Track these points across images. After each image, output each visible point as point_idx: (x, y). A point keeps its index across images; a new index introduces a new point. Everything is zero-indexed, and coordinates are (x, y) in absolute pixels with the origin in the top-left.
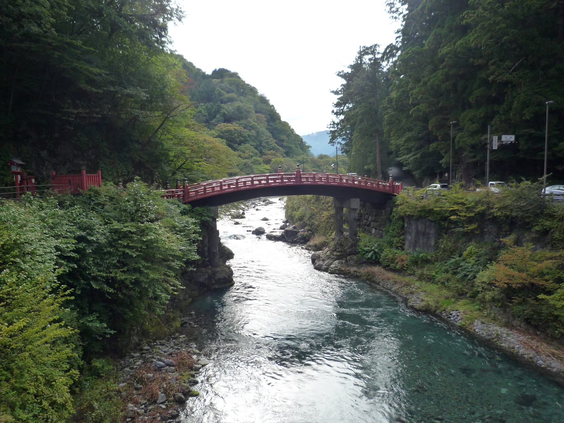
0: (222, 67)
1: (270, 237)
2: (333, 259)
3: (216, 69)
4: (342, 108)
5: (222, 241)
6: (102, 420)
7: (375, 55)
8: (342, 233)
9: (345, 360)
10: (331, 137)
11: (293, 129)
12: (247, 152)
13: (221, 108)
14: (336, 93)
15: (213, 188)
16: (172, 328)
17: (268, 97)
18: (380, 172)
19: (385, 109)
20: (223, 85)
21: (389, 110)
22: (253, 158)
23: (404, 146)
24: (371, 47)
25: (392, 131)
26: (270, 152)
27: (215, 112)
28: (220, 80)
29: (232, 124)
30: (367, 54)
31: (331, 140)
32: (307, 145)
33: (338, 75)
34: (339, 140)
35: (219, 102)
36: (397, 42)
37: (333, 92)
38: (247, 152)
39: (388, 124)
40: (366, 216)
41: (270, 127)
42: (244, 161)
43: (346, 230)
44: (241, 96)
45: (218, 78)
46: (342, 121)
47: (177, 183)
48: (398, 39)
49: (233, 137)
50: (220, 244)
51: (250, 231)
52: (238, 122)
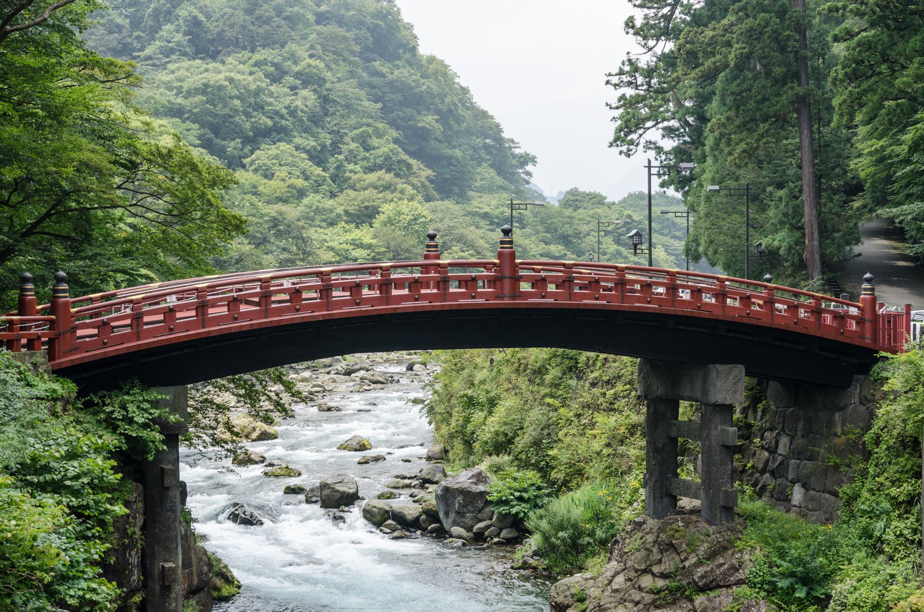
4: (666, 10)
6: (749, 607)
8: (674, 500)
11: (465, 91)
12: (282, 172)
18: (818, 263)
21: (850, 23)
22: (305, 201)
23: (907, 162)
25: (861, 106)
26: (372, 177)
31: (620, 130)
32: (517, 151)
34: (654, 134)
38: (282, 172)
39: (853, 77)
42: (272, 210)
43: (688, 490)
46: (668, 60)
50: (190, 538)
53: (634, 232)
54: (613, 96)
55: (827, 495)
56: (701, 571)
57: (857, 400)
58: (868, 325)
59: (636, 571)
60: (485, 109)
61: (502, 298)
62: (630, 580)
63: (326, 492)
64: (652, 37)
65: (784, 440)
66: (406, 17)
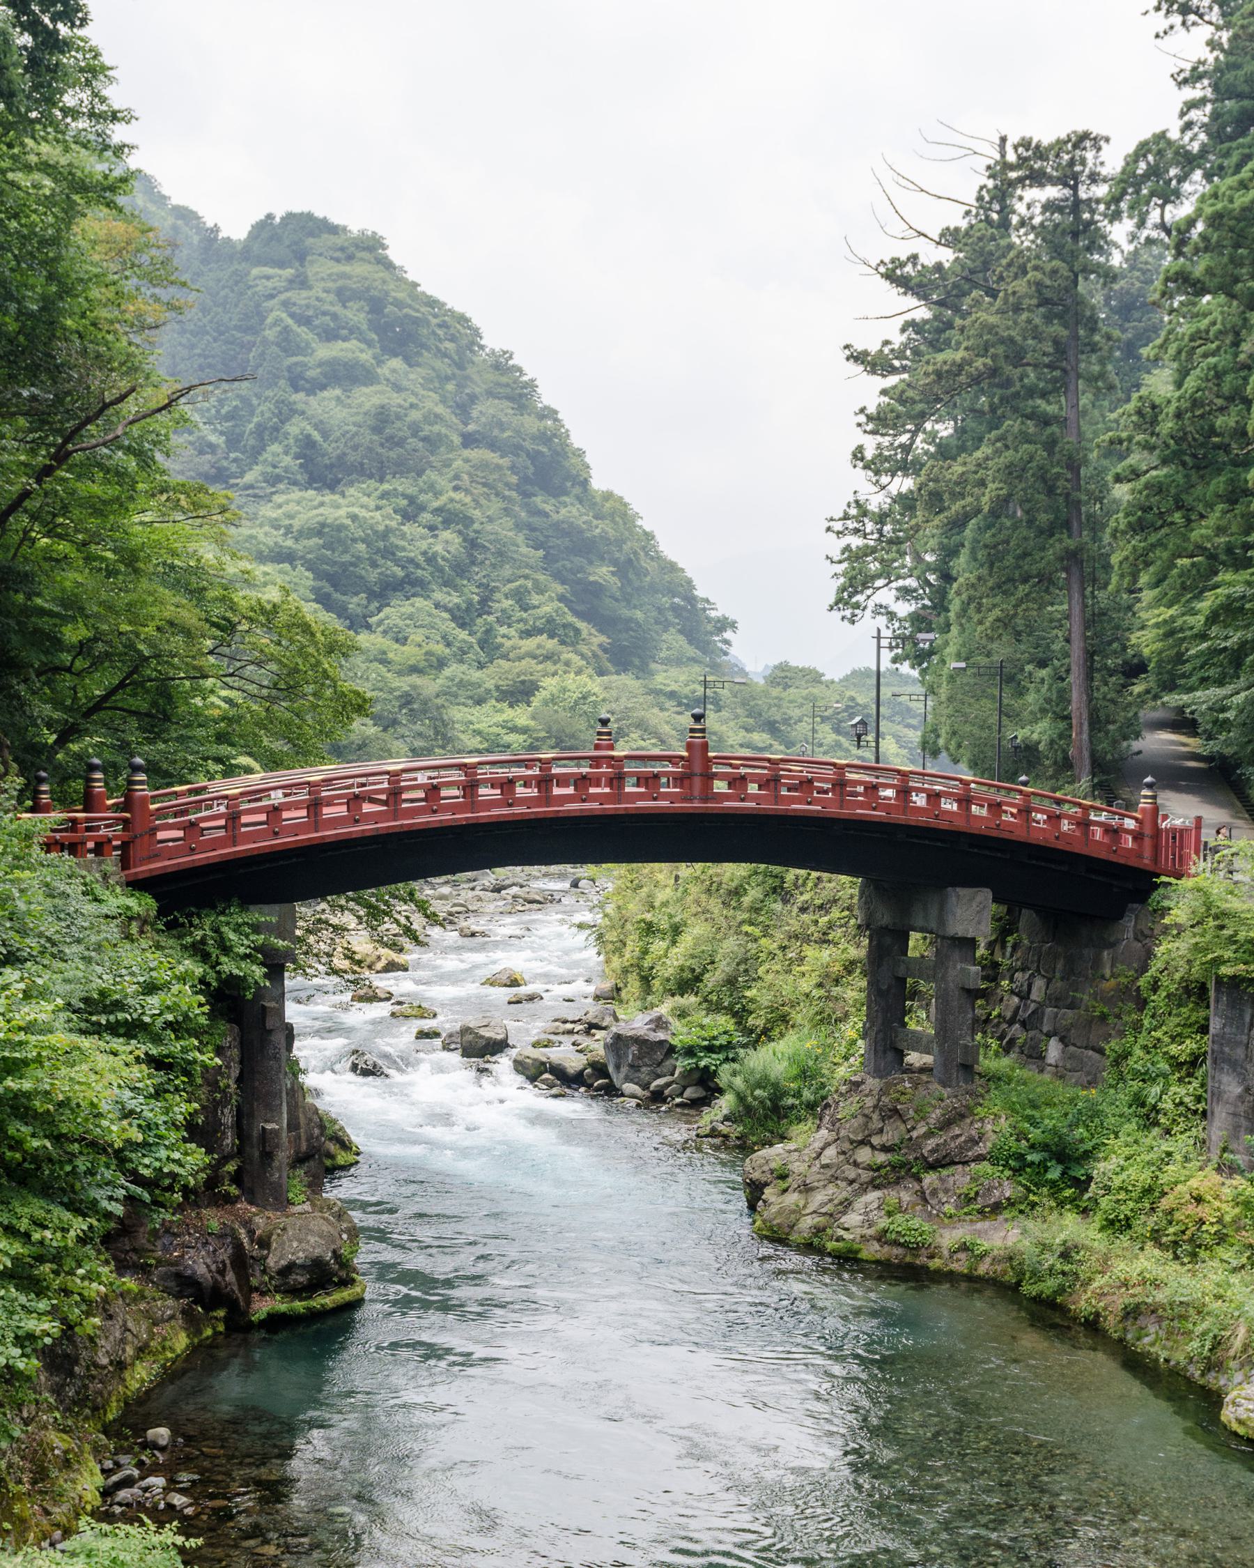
1: (533, 1072)
2: (851, 1182)
3: (270, 217)
4: (904, 439)
5: (310, 1080)
7: (1075, 188)
8: (900, 1055)
12: (417, 636)
13: (293, 412)
15: (275, 811)
16: (56, 1503)
17: (530, 364)
18: (1087, 762)
19: (1116, 448)
20: (299, 297)
21: (1137, 458)
22: (447, 672)
24: (1060, 144)
26: (530, 644)
27: (260, 430)
28: (289, 272)
29: (343, 495)
30: (1038, 178)
32: (713, 614)
33: (890, 276)
35: (282, 382)
36: (1188, 126)
37: (858, 357)
39: (1139, 527)
40: (1018, 975)
41: (536, 521)
42: (403, 684)
43: (918, 1043)
44: (395, 354)
45: (281, 265)
46: (906, 502)
47: (89, 780)
48: (1195, 115)
49: (346, 558)
50: (297, 1091)
51: (434, 1034)
52: (372, 483)
53: (857, 719)
54: (835, 546)
55: (1091, 1053)
56: (931, 1143)
57: (1131, 935)
58: (1147, 842)
59: (852, 1142)
61: (691, 801)
62: (844, 1153)
63: (469, 1037)
64: (886, 472)
65: (1039, 983)
66: (576, 441)
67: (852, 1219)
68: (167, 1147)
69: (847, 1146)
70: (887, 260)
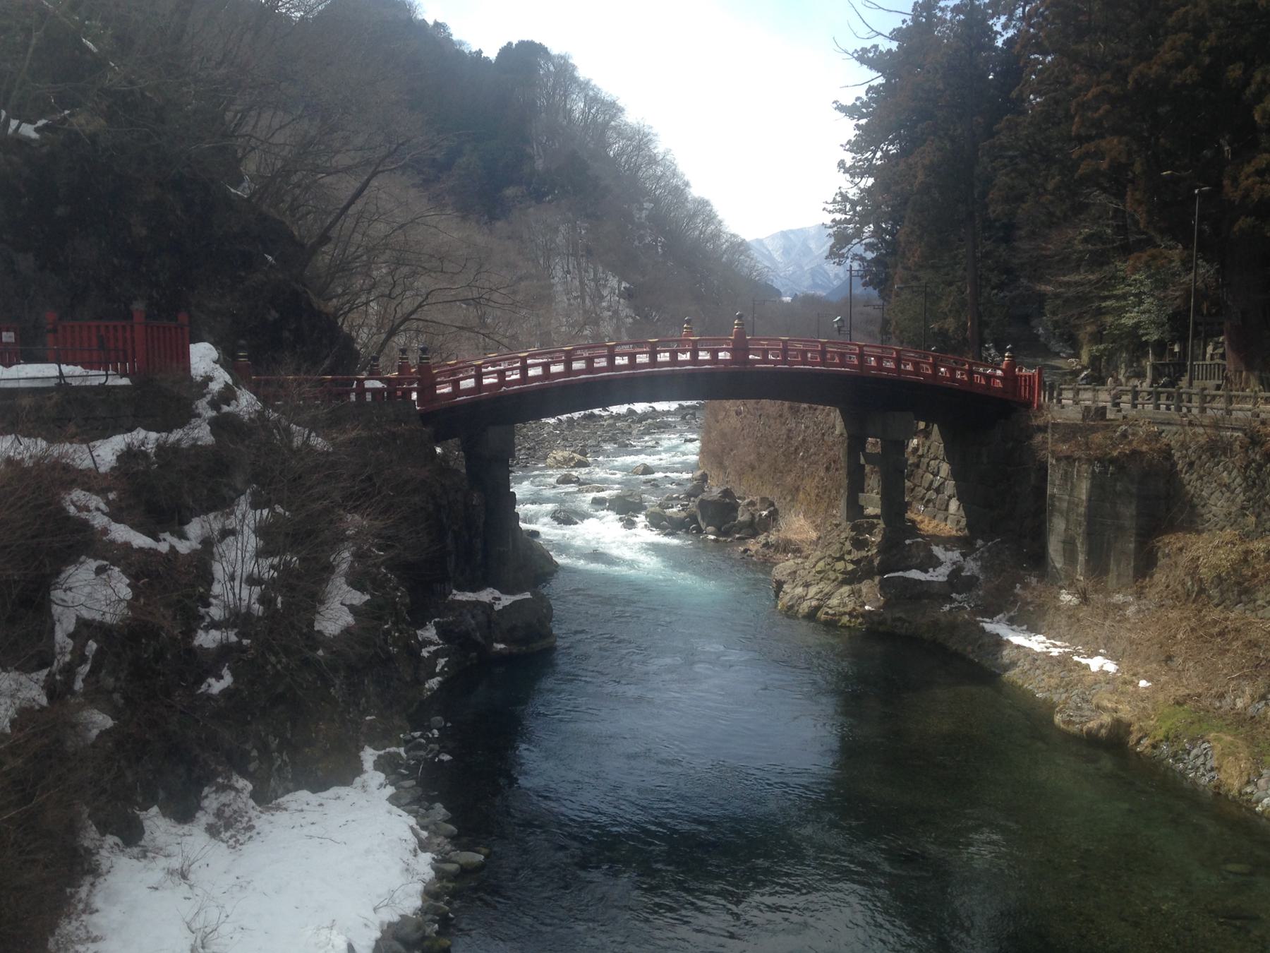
0: (527, 37)
3: (510, 44)
9: (340, 222)
10: (832, 241)
14: (851, 111)
31: (832, 247)
37: (841, 108)
55: (528, 506)
59: (834, 558)
60: (530, 39)
64: (858, 174)
67: (834, 601)
68: (1060, 711)
69: (829, 560)
70: (858, 50)
